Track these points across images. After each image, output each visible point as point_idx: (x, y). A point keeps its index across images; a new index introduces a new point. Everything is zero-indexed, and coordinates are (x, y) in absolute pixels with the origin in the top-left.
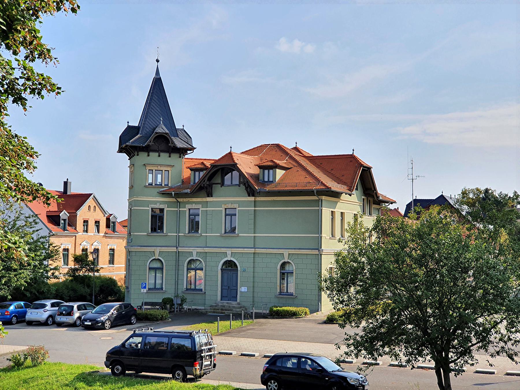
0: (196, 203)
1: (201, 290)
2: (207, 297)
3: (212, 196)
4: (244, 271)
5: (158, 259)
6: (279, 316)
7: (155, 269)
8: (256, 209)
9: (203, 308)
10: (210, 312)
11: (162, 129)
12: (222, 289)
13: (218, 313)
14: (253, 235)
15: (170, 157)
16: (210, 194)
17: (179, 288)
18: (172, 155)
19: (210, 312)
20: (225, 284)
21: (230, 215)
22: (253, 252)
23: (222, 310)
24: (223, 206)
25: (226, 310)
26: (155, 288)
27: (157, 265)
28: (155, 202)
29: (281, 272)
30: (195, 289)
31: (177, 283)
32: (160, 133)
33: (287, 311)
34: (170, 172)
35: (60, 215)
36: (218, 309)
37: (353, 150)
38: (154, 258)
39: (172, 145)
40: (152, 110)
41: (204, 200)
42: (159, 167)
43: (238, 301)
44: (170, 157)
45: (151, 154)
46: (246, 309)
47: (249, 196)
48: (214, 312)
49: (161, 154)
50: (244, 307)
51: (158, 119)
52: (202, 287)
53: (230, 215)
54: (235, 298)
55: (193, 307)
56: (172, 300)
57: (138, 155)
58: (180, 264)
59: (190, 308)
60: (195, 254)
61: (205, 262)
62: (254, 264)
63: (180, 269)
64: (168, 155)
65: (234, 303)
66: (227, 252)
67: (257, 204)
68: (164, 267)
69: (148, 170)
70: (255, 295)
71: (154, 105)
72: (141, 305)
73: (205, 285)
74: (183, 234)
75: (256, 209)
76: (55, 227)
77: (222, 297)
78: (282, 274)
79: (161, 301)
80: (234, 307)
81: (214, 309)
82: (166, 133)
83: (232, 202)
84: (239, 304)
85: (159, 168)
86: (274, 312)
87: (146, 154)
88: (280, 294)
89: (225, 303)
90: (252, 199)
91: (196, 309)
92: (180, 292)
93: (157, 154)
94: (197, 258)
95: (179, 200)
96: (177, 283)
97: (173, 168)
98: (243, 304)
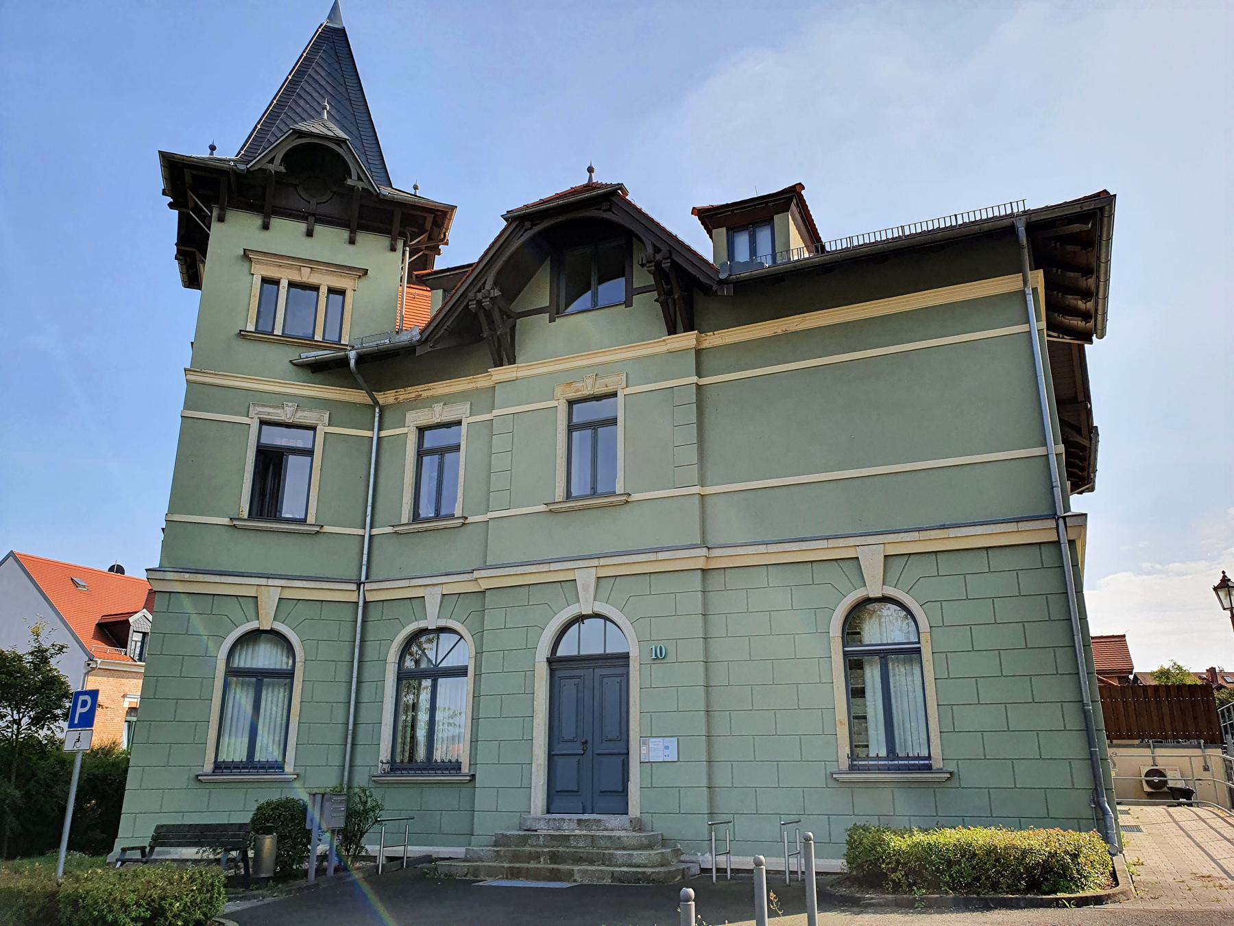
0: (447, 400)
1: (456, 767)
2: (483, 800)
3: (512, 361)
4: (660, 657)
5: (272, 632)
6: (934, 886)
7: (259, 678)
8: (705, 381)
9: (459, 851)
10: (492, 872)
11: (324, 125)
12: (551, 757)
13: (536, 875)
14: (696, 490)
15: (352, 242)
16: (505, 354)
17: (358, 761)
18: (362, 237)
19: (492, 872)
20: (568, 730)
21: (590, 421)
22: (701, 564)
23: (554, 857)
24: (559, 391)
25: (578, 860)
26: (250, 764)
27: (264, 657)
28: (279, 400)
29: (845, 654)
30: (430, 765)
31: (352, 740)
32: (311, 135)
33: (991, 851)
34: (349, 294)
35: (131, 620)
36: (536, 857)
37: (590, 170)
38: (253, 625)
39: (360, 185)
40: (302, 103)
41: (482, 381)
42: (306, 271)
43: (634, 810)
44: (352, 242)
45: (275, 222)
46: (677, 853)
47: (672, 331)
48: (514, 873)
49: (319, 229)
50: (664, 842)
51: (315, 105)
52: (461, 752)
53: (590, 421)
54: (617, 798)
55: (415, 850)
56: (304, 810)
57: (221, 219)
58: (371, 653)
59: (397, 851)
60: (432, 604)
61: (479, 636)
62: (705, 622)
63: (367, 676)
64: (345, 234)
65: (614, 824)
66: (577, 575)
67: (708, 362)
68: (299, 666)
69: (257, 281)
70: (721, 779)
71: (308, 89)
72: (146, 843)
73: (474, 741)
74: (389, 530)
75: (705, 381)
76: (109, 649)
77: (555, 795)
78: (854, 664)
79: (248, 821)
80: (618, 844)
81: (516, 857)
82: (339, 141)
83: (598, 371)
84: (638, 825)
85: (306, 276)
86: (900, 859)
87: (258, 221)
88: (852, 768)
89: (569, 824)
90: (686, 340)
91: (428, 859)
92: (361, 779)
93: (302, 227)
94: (442, 623)
95: (382, 398)
96: (352, 740)
97: (363, 283)
98: (661, 826)
